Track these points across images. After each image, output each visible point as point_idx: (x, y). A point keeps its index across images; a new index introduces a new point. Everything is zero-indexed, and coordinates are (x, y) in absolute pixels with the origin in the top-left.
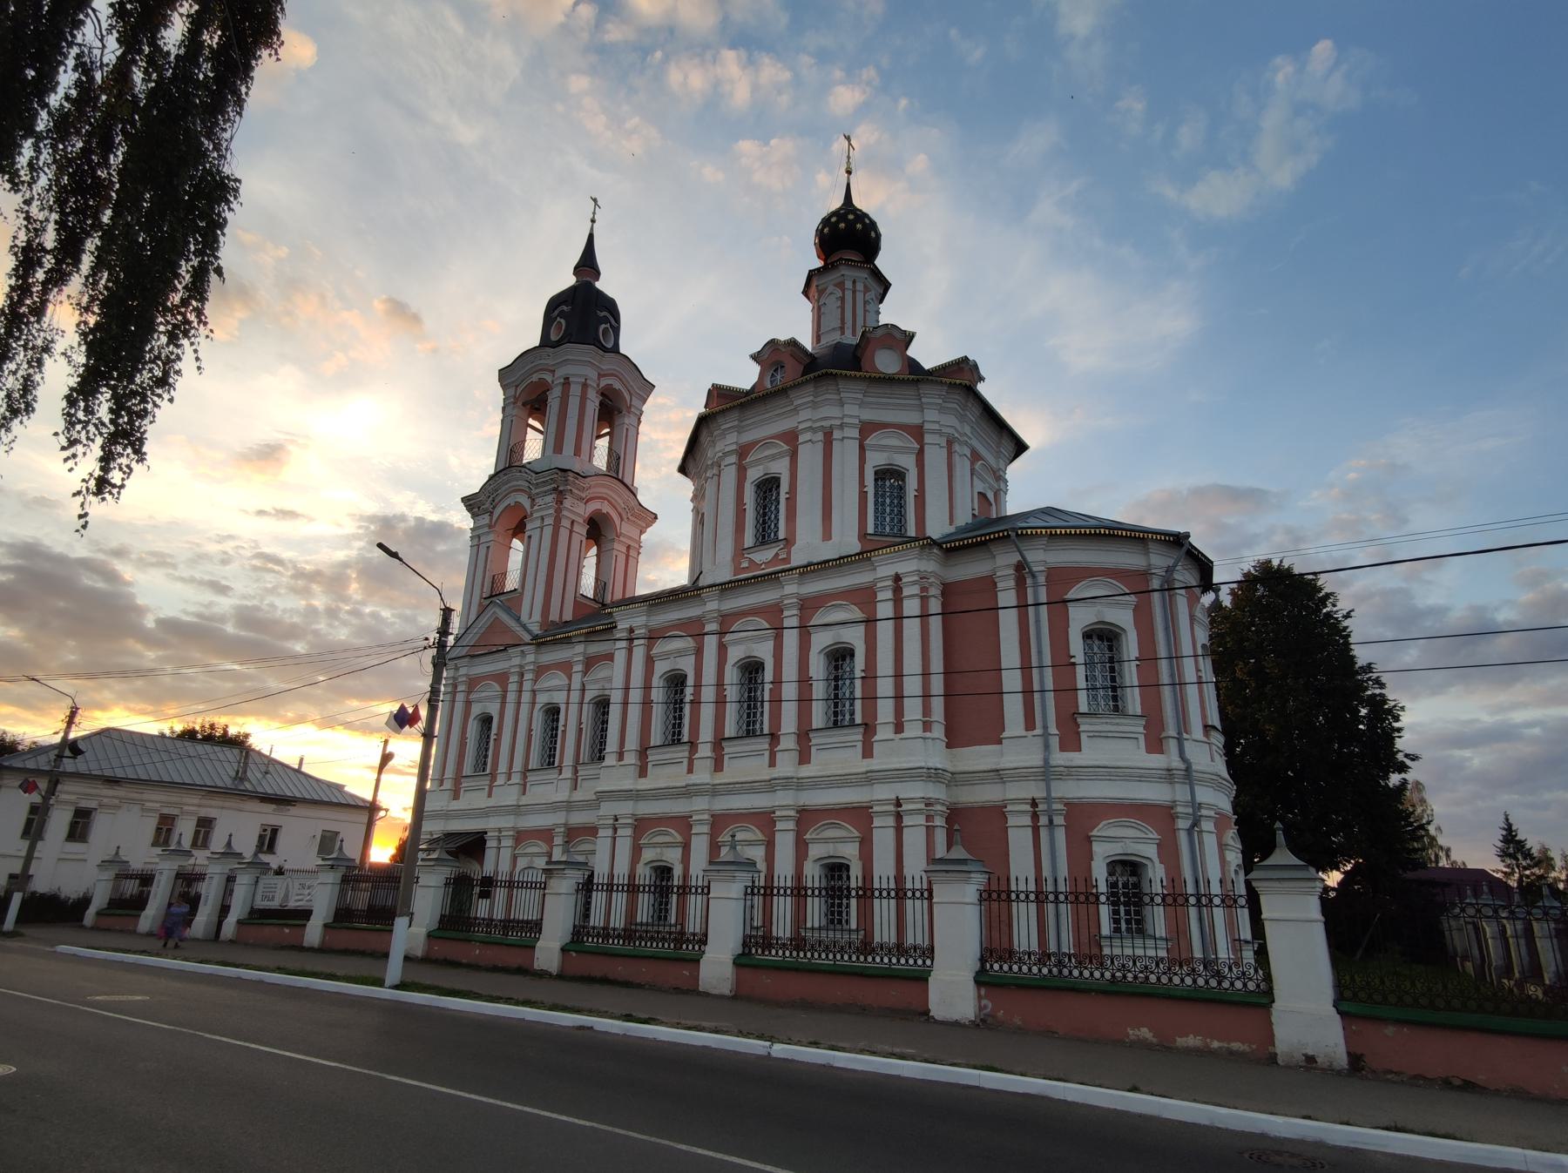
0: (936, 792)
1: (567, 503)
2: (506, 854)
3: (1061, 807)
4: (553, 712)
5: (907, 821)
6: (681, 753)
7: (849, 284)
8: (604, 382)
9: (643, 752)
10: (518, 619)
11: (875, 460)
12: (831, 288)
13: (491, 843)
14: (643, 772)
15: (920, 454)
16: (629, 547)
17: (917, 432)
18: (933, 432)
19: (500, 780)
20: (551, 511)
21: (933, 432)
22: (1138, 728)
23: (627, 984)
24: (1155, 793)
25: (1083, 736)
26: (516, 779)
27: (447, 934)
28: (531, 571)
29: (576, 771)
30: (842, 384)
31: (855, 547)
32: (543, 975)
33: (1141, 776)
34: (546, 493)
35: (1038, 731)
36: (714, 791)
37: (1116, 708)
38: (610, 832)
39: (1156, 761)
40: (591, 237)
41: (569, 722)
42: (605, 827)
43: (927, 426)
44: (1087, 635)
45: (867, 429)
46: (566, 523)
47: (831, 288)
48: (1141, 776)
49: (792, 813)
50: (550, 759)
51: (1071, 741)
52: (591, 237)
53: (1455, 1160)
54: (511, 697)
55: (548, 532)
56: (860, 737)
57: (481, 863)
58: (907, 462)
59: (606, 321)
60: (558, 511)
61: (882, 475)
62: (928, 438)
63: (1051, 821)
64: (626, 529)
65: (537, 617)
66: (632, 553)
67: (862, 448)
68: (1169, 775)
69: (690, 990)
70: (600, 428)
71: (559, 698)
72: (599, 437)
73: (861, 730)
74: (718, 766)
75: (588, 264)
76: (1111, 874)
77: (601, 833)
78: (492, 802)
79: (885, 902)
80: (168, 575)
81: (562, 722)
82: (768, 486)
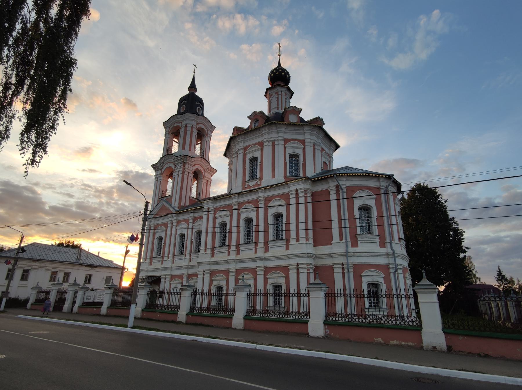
0: (310, 261)
2: (167, 283)
4: (183, 236)
5: (301, 271)
6: (226, 249)
9: (213, 249)
10: (171, 205)
11: (289, 151)
15: (304, 149)
16: (207, 181)
17: (303, 142)
18: (308, 142)
19: (165, 259)
20: (181, 169)
21: (308, 142)
22: (377, 239)
23: (208, 326)
25: (359, 242)
26: (171, 258)
28: (175, 190)
32: (180, 323)
33: (378, 255)
34: (179, 163)
35: (344, 241)
36: (237, 262)
37: (370, 233)
38: (202, 276)
41: (188, 239)
42: (200, 274)
43: (306, 140)
44: (360, 209)
45: (286, 141)
46: (186, 173)
48: (378, 255)
49: (263, 269)
50: (182, 252)
51: (355, 244)
54: (169, 231)
55: (180, 176)
56: (285, 243)
58: (300, 152)
60: (184, 169)
61: (291, 156)
62: (307, 144)
63: (348, 270)
64: (206, 175)
65: (177, 204)
66: (209, 183)
67: (285, 147)
68: (387, 255)
69: (230, 328)
70: (197, 141)
71: (185, 231)
72: (197, 144)
73: (285, 241)
74: (238, 253)
75: (193, 87)
76: (368, 288)
77: (199, 276)
78: (163, 266)
81: (186, 239)
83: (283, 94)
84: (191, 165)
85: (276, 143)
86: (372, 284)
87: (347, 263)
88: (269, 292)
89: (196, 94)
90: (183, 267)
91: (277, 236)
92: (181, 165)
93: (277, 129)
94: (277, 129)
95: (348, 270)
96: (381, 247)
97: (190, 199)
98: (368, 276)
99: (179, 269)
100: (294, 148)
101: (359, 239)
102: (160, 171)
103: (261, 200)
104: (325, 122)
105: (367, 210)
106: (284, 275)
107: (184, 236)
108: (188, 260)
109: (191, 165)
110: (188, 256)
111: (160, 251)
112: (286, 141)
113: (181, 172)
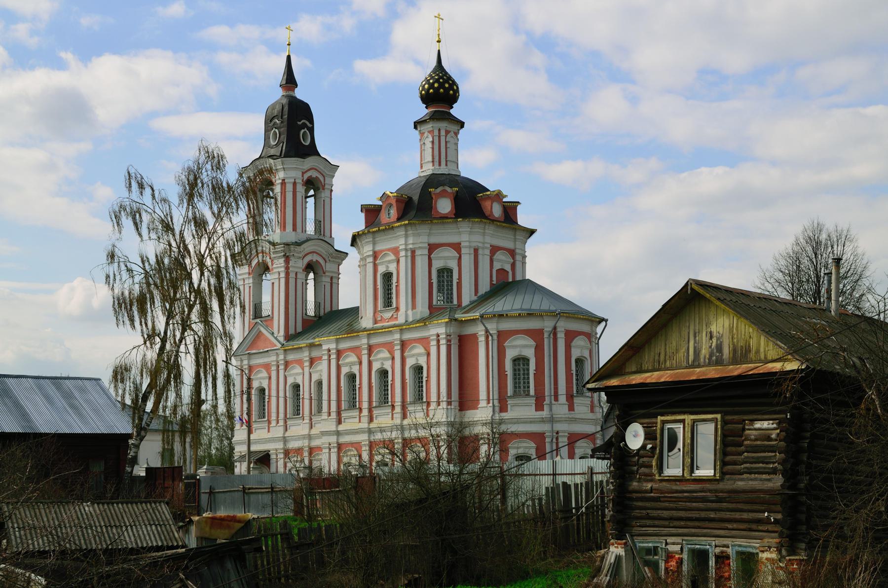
0: (333, 439)
1: (291, 263)
2: (281, 463)
6: (355, 413)
7: (436, 133)
8: (306, 176)
9: (339, 413)
10: (273, 334)
11: (437, 264)
13: (273, 457)
14: (339, 422)
15: (460, 259)
16: (332, 278)
17: (457, 247)
18: (466, 247)
19: (273, 423)
20: (283, 269)
21: (466, 247)
22: (533, 401)
26: (281, 423)
28: (276, 305)
29: (311, 419)
30: (417, 226)
31: (426, 312)
33: (532, 421)
34: (279, 257)
35: (491, 405)
38: (327, 450)
39: (540, 414)
40: (289, 57)
41: (305, 393)
42: (325, 448)
43: (463, 244)
45: (432, 248)
46: (292, 275)
47: (452, 134)
48: (532, 421)
50: (297, 411)
51: (503, 408)
52: (289, 57)
54: (274, 375)
55: (283, 281)
57: (269, 467)
58: (453, 265)
59: (304, 126)
60: (287, 268)
61: (441, 271)
62: (463, 251)
64: (329, 267)
65: (282, 333)
66: (334, 281)
68: (542, 421)
70: (307, 191)
71: (299, 380)
72: (307, 197)
74: (371, 420)
75: (290, 81)
77: (324, 451)
78: (270, 435)
81: (301, 393)
82: (388, 276)
83: (443, 133)
84: (300, 258)
85: (480, 252)
90: (303, 437)
92: (282, 260)
93: (484, 229)
97: (303, 320)
99: (296, 440)
100: (445, 258)
101: (510, 402)
102: (246, 267)
103: (397, 345)
104: (505, 193)
107: (298, 386)
108: (308, 426)
109: (300, 258)
110: (307, 420)
111: (264, 410)
112: (494, 250)
113: (283, 275)
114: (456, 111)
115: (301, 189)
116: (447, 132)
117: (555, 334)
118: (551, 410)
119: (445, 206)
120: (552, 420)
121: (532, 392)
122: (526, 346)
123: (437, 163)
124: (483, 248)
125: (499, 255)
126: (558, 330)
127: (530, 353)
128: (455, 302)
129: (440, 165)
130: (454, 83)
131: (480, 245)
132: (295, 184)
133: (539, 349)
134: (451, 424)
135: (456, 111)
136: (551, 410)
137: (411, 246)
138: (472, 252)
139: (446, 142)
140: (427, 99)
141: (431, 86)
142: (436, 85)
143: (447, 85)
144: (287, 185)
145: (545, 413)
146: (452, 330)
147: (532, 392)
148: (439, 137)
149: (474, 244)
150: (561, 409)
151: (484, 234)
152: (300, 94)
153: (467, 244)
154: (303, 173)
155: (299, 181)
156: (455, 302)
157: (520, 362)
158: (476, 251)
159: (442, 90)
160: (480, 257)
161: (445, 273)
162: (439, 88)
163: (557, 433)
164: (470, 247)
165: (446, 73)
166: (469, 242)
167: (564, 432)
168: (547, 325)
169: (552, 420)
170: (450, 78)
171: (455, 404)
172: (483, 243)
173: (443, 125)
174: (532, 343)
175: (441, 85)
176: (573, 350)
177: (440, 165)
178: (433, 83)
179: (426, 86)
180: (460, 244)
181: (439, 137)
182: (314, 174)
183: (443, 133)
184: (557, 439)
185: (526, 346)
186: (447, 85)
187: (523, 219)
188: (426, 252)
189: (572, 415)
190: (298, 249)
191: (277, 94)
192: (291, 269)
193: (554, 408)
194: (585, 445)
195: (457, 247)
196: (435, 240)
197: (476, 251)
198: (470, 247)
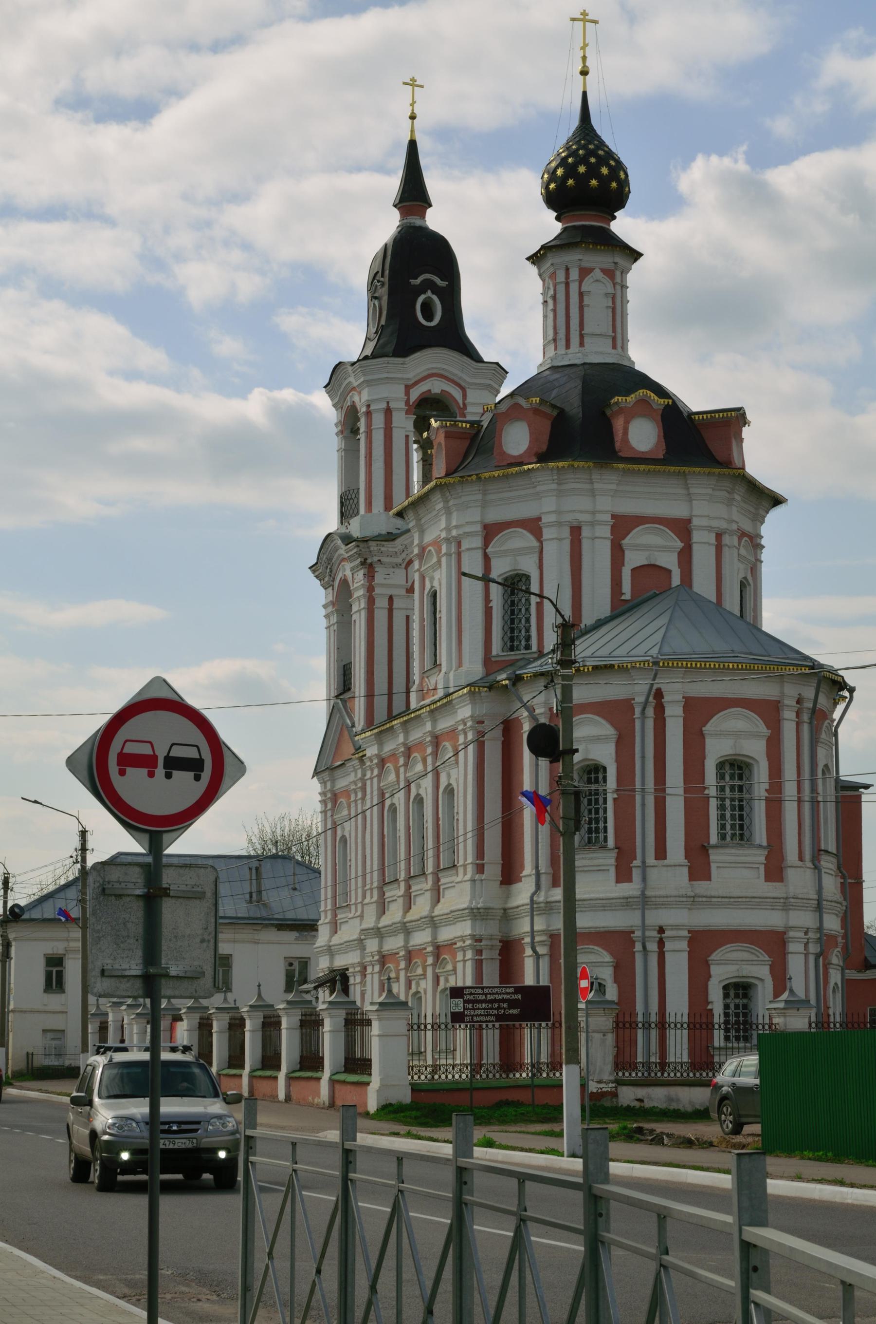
1: (379, 578)
3: (544, 938)
5: (668, 946)
7: (561, 276)
8: (415, 394)
12: (597, 274)
17: (533, 526)
22: (759, 857)
24: (771, 919)
25: (713, 866)
27: (587, 1099)
36: (694, 902)
37: (742, 836)
43: (545, 519)
44: (720, 766)
45: (490, 531)
46: (381, 603)
47: (597, 274)
49: (685, 933)
53: (663, 1178)
56: (613, 861)
60: (370, 589)
63: (644, 947)
68: (626, 903)
73: (614, 854)
76: (726, 996)
79: (679, 1032)
80: (378, 272)
85: (585, 533)
86: (736, 986)
87: (644, 927)
88: (755, 1022)
89: (555, 214)
91: (741, 818)
93: (591, 482)
94: (591, 482)
95: (644, 947)
96: (769, 878)
98: (727, 962)
100: (513, 554)
101: (715, 856)
104: (749, 416)
105: (740, 768)
106: (767, 958)
112: (622, 526)
114: (623, 225)
115: (404, 424)
116: (585, 272)
117: (660, 709)
118: (644, 879)
119: (642, 435)
120: (644, 902)
121: (611, 842)
122: (597, 739)
123: (562, 343)
124: (592, 524)
125: (636, 538)
126: (667, 698)
127: (755, 749)
128: (534, 648)
129: (568, 346)
130: (619, 162)
131: (584, 518)
132: (388, 412)
133: (624, 744)
134: (477, 914)
135: (623, 225)
136: (644, 879)
137: (454, 533)
138: (566, 533)
139: (581, 295)
140: (558, 198)
141: (571, 171)
142: (582, 169)
143: (605, 171)
144: (374, 416)
145: (631, 889)
146: (483, 709)
147: (611, 842)
148: (567, 284)
149: (569, 517)
150: (670, 877)
151: (593, 493)
152: (435, 220)
153: (552, 518)
154: (408, 388)
155: (399, 405)
156: (534, 648)
157: (736, 768)
158: (576, 531)
159: (594, 182)
160: (586, 545)
161: (516, 585)
162: (565, 177)
163: (661, 930)
164: (559, 524)
165: (602, 144)
166: (558, 512)
167: (677, 927)
168: (638, 689)
169: (644, 902)
170: (610, 154)
171: (494, 870)
172: (593, 513)
173: (598, 260)
174: (608, 730)
175: (593, 171)
176: (708, 741)
177: (568, 346)
178: (575, 165)
179: (560, 172)
180: (689, 521)
181: (567, 284)
182: (436, 387)
183: (574, 274)
184: (661, 943)
185: (597, 739)
186: (605, 171)
187: (760, 455)
188: (478, 542)
189: (701, 887)
190: (388, 547)
191: (387, 225)
192: (377, 591)
193: (286, 889)
194: (745, 956)
195: (533, 526)
196: (495, 515)
197: (576, 531)
198: (559, 524)
